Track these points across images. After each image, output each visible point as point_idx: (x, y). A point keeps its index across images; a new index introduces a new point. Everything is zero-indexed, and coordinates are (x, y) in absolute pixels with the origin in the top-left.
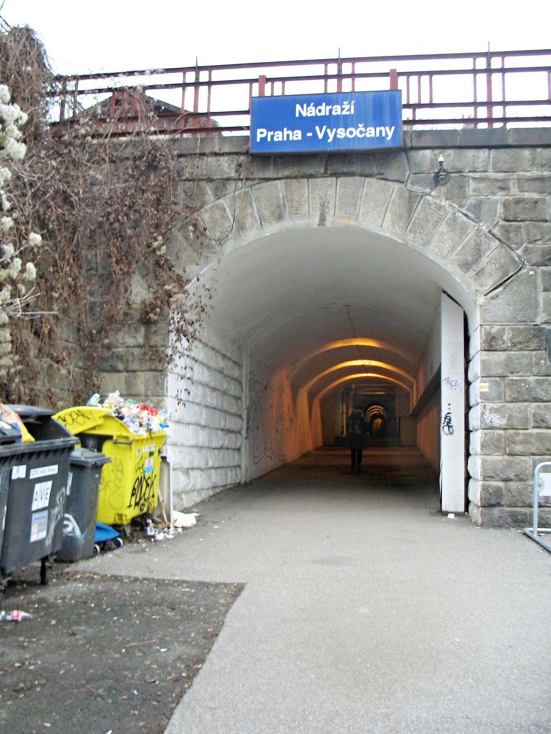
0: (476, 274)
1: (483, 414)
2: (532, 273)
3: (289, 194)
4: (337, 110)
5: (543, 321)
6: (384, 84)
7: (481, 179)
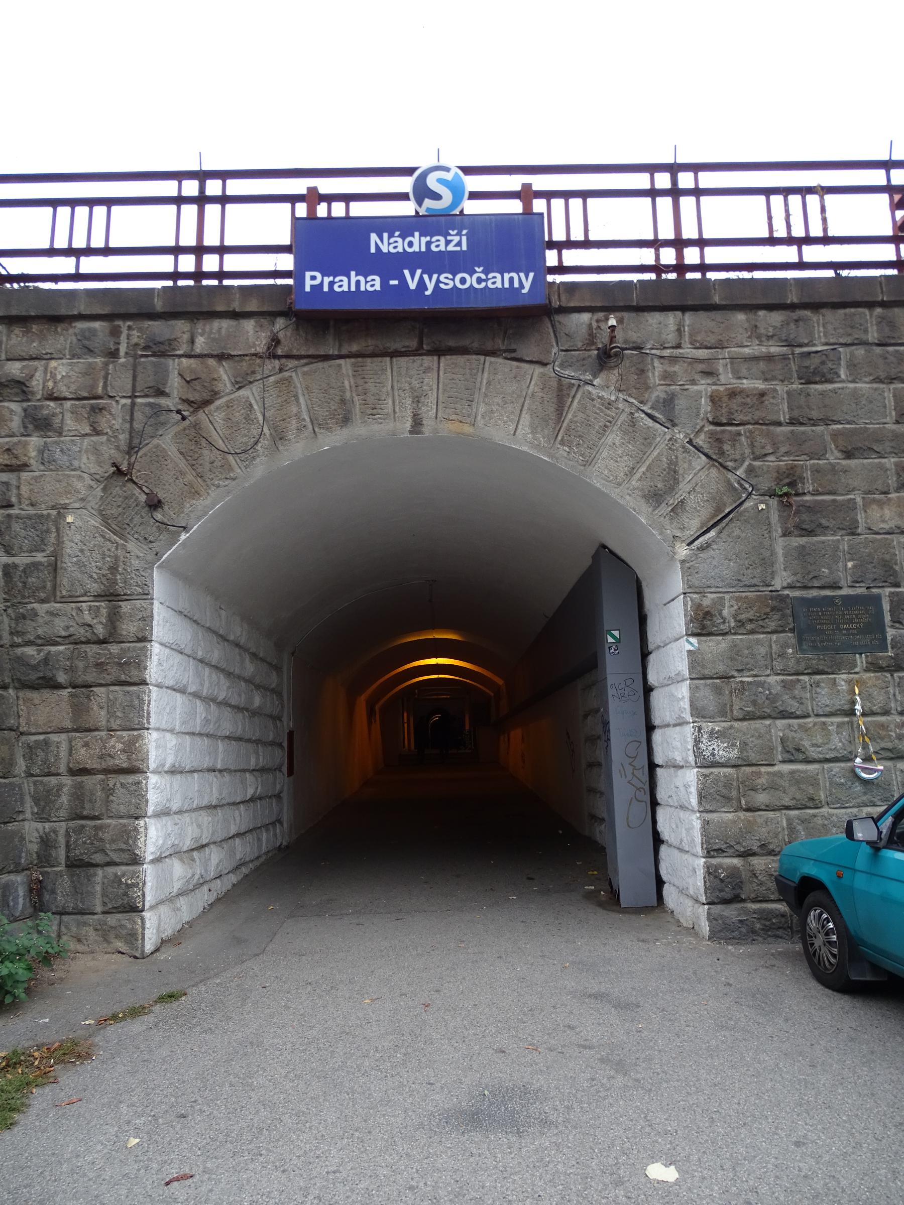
0: (672, 510)
1: (697, 741)
2: (762, 506)
3: (360, 382)
4: (439, 244)
5: (785, 584)
6: (515, 207)
7: (673, 359)
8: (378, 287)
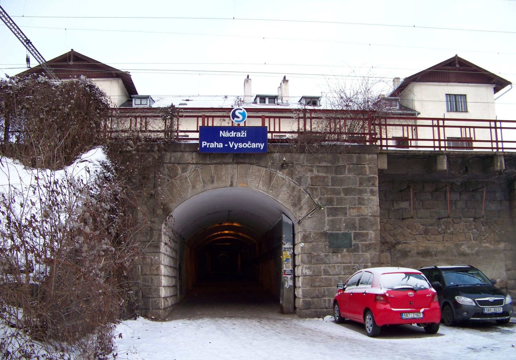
1: (302, 270)
4: (239, 135)
8: (222, 147)
